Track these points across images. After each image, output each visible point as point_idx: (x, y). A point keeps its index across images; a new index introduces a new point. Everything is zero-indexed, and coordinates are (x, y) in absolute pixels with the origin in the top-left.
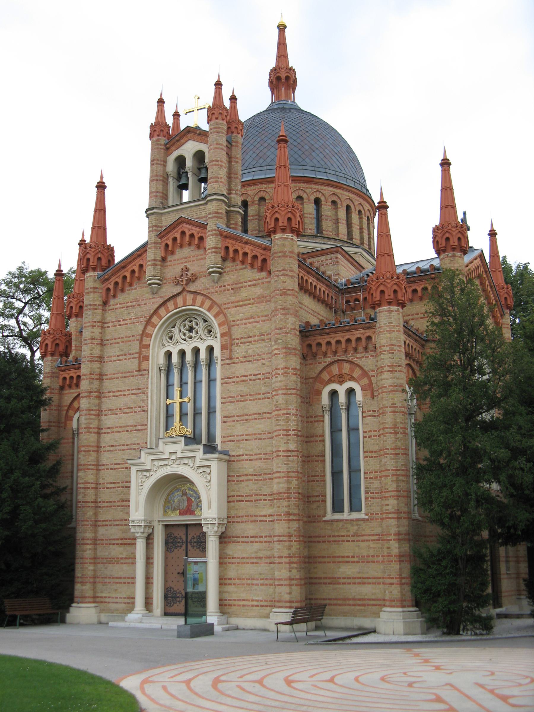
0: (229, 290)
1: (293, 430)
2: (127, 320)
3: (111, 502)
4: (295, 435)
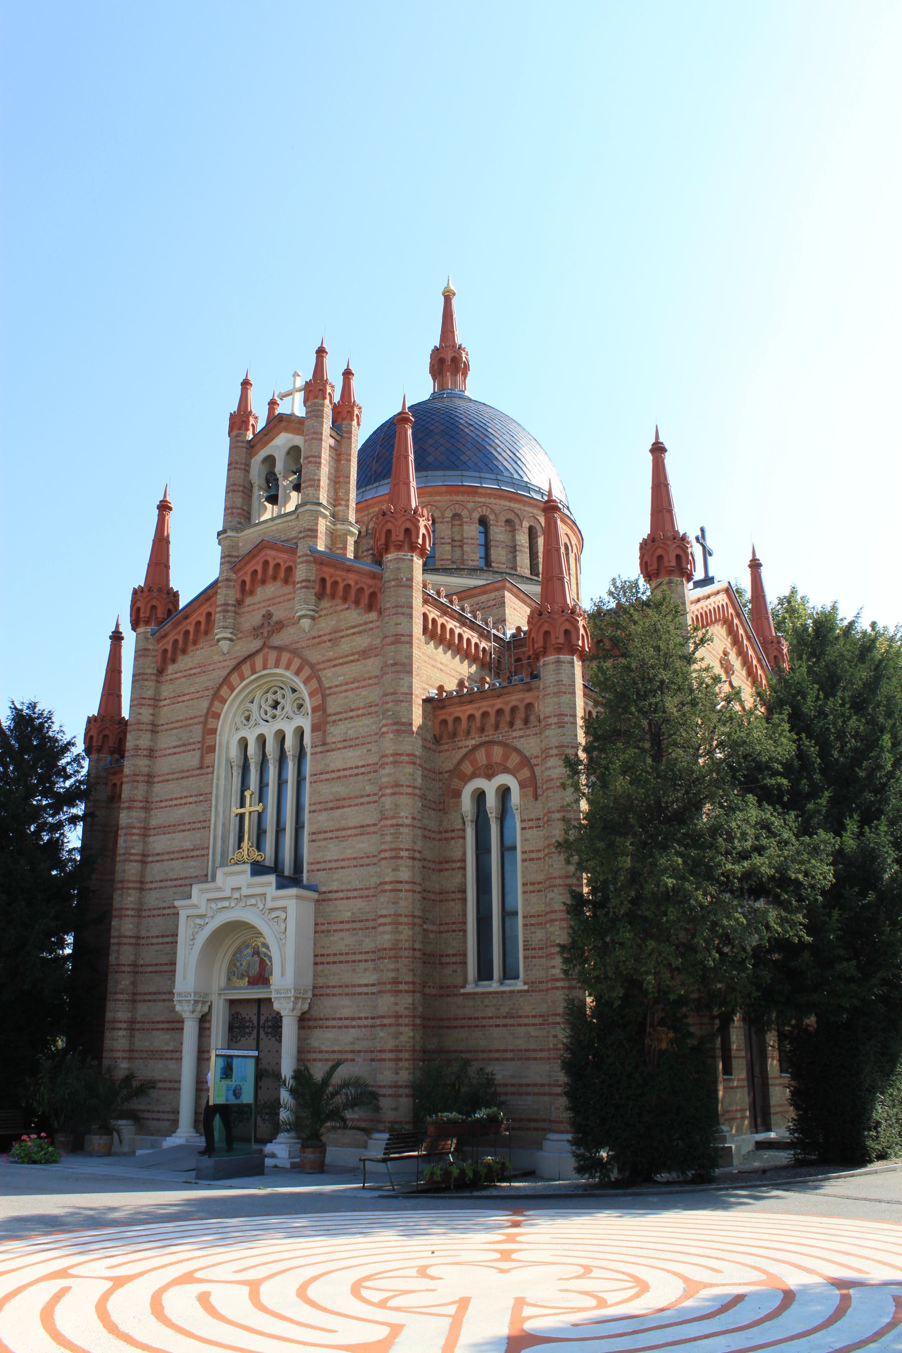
0: (325, 642)
1: (407, 850)
2: (188, 694)
3: (156, 965)
4: (409, 858)
